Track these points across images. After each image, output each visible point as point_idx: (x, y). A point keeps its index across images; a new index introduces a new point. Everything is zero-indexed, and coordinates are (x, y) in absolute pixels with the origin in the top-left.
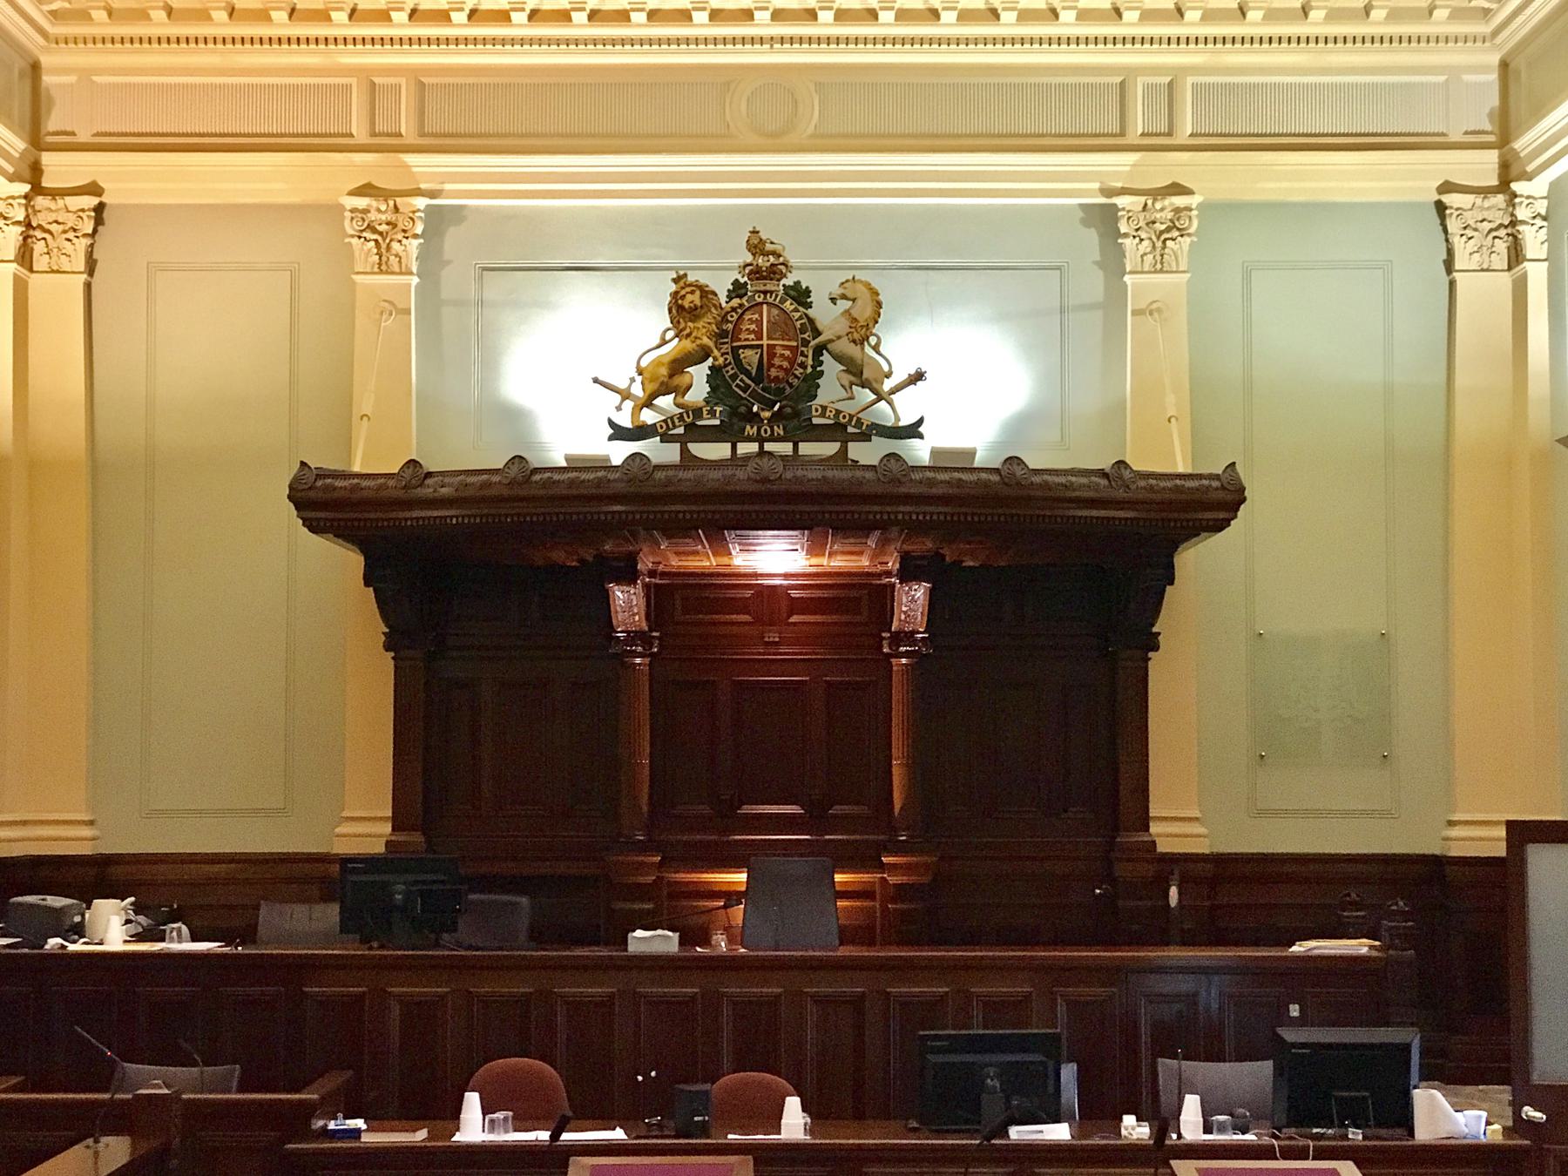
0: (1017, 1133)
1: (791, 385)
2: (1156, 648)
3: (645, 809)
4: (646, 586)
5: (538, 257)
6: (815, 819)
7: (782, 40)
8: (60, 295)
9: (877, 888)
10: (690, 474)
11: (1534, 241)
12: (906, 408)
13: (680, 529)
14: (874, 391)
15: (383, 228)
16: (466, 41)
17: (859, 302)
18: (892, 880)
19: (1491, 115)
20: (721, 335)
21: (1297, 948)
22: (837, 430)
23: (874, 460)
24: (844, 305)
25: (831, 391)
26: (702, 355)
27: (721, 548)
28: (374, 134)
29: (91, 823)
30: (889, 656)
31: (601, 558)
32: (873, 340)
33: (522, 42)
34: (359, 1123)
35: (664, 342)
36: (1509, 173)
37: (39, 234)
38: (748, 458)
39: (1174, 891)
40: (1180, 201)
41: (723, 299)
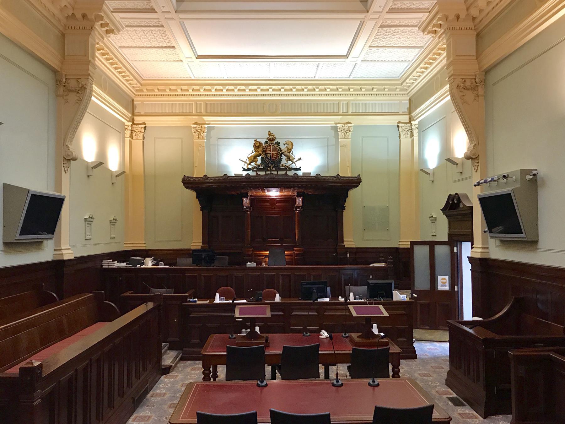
0: (319, 300)
5: (227, 136)
8: (137, 144)
11: (415, 132)
13: (256, 188)
20: (263, 151)
22: (286, 169)
25: (284, 161)
27: (263, 190)
33: (225, 95)
34: (196, 299)
38: (268, 174)
40: (349, 125)
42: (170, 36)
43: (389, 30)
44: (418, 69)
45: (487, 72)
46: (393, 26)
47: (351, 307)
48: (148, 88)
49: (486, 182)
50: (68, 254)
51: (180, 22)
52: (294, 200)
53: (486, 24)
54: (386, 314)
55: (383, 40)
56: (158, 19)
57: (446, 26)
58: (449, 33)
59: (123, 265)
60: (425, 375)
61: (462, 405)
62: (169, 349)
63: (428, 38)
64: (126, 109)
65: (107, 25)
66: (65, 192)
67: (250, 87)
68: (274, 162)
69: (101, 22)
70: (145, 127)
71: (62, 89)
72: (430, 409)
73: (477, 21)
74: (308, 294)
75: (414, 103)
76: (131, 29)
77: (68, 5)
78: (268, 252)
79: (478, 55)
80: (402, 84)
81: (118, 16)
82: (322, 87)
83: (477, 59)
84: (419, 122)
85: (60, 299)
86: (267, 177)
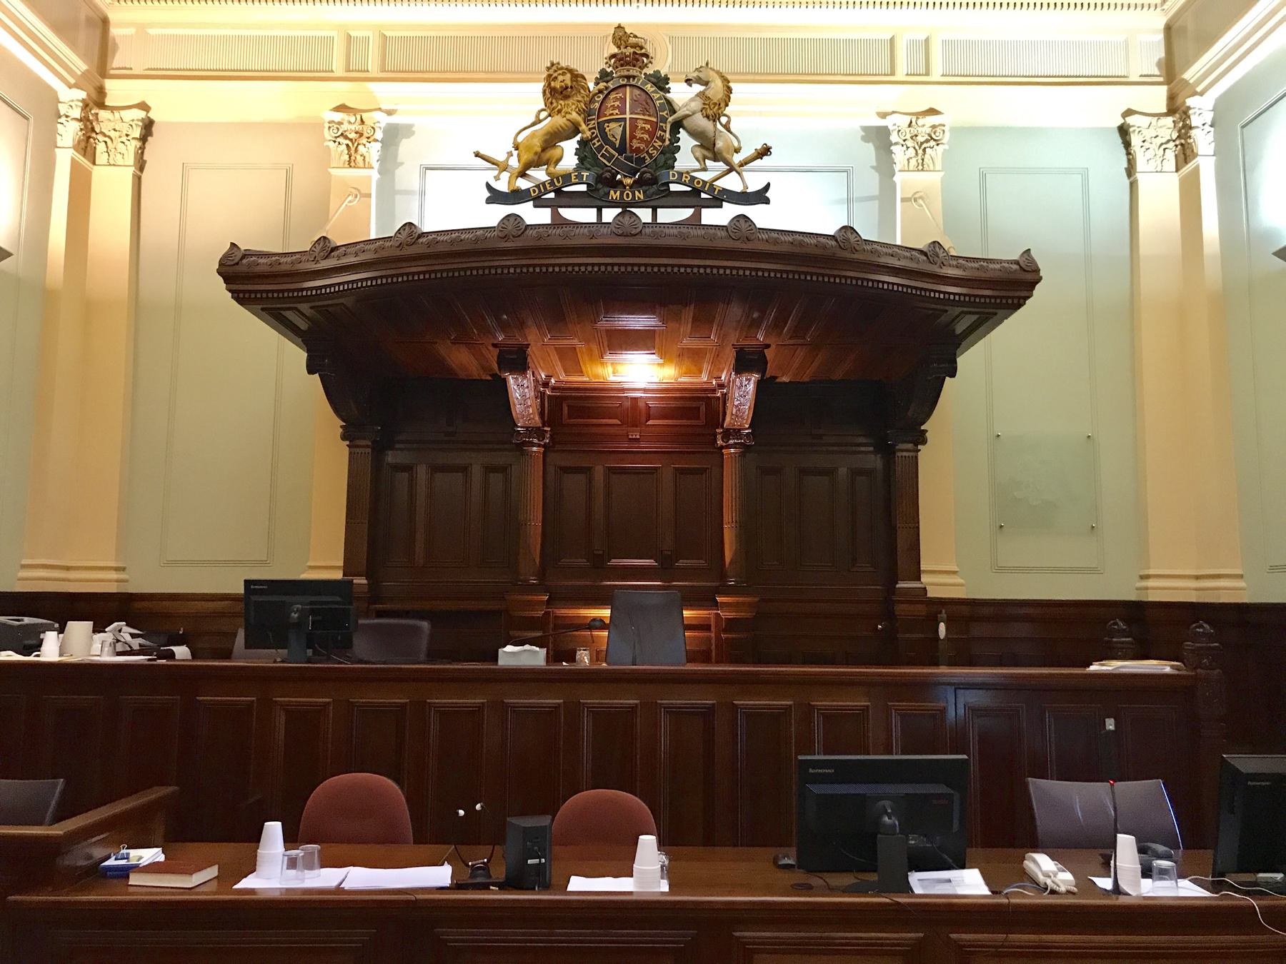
1: (651, 156)
2: (924, 442)
3: (538, 561)
6: (666, 569)
9: (713, 623)
11: (1203, 140)
14: (727, 163)
15: (352, 136)
17: (712, 85)
18: (724, 614)
19: (1159, 64)
20: (587, 114)
21: (1095, 668)
23: (724, 221)
24: (698, 88)
25: (686, 159)
28: (348, 70)
29: (117, 569)
30: (722, 447)
32: (724, 120)
35: (538, 121)
37: (100, 137)
39: (942, 627)
41: (591, 85)
74: (848, 844)
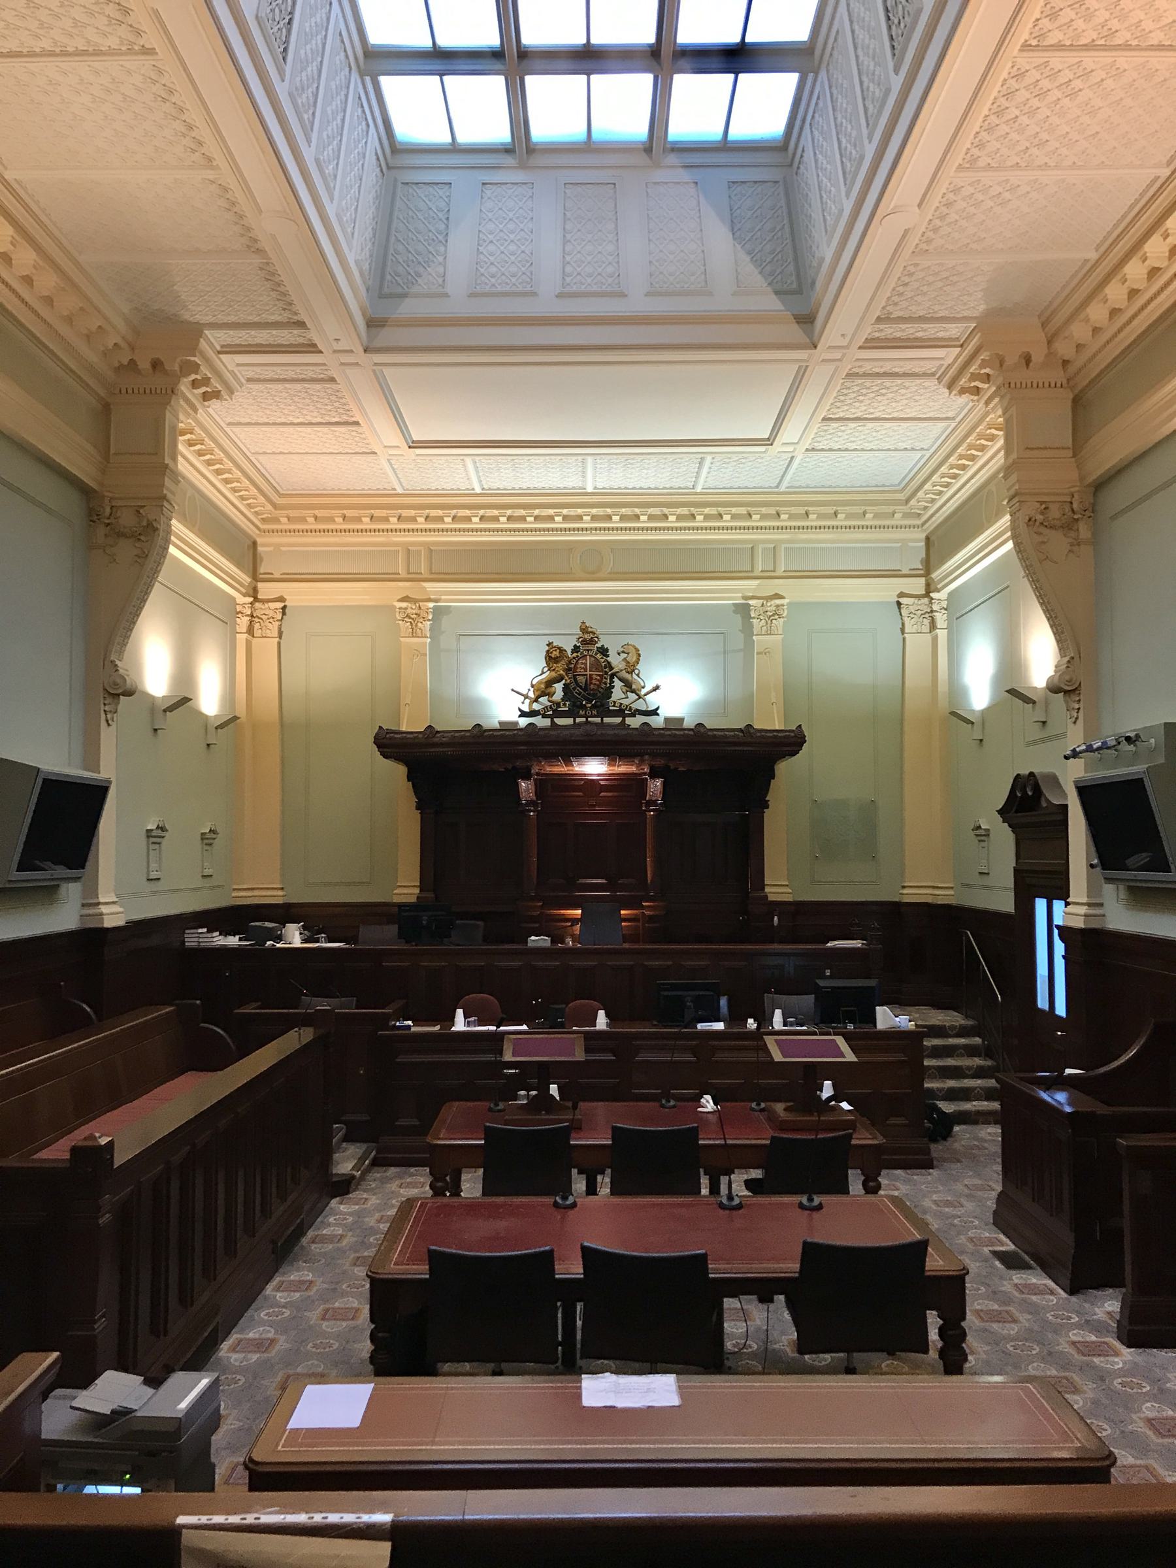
0: (700, 1026)
4: (535, 780)
5: (484, 631)
7: (596, 529)
8: (266, 647)
10: (552, 733)
11: (941, 619)
12: (653, 701)
13: (551, 757)
16: (451, 530)
19: (921, 562)
20: (567, 670)
22: (621, 712)
25: (618, 693)
26: (558, 680)
27: (568, 763)
29: (282, 889)
31: (514, 768)
33: (477, 530)
34: (410, 1023)
35: (543, 673)
36: (929, 589)
38: (580, 724)
40: (778, 602)
42: (352, 406)
43: (868, 384)
44: (943, 469)
45: (1100, 486)
46: (878, 375)
47: (770, 1041)
48: (292, 513)
49: (1090, 749)
50: (113, 916)
51: (374, 371)
52: (643, 785)
53: (1094, 375)
54: (850, 1057)
55: (857, 404)
56: (324, 364)
57: (1000, 380)
58: (1008, 396)
59: (233, 941)
60: (948, 1204)
61: (1025, 1267)
62: (347, 1138)
63: (960, 403)
64: (238, 565)
65: (206, 381)
66: (106, 771)
67: (537, 512)
68: (594, 695)
69: (193, 377)
70: (284, 608)
71: (101, 531)
72: (920, 1248)
73: (1072, 369)
75: (939, 545)
76: (260, 386)
77: (123, 344)
78: (579, 912)
79: (1077, 448)
80: (907, 501)
81: (230, 361)
82: (712, 511)
83: (1074, 456)
84: (950, 594)
85: (100, 1020)
86: (577, 732)
